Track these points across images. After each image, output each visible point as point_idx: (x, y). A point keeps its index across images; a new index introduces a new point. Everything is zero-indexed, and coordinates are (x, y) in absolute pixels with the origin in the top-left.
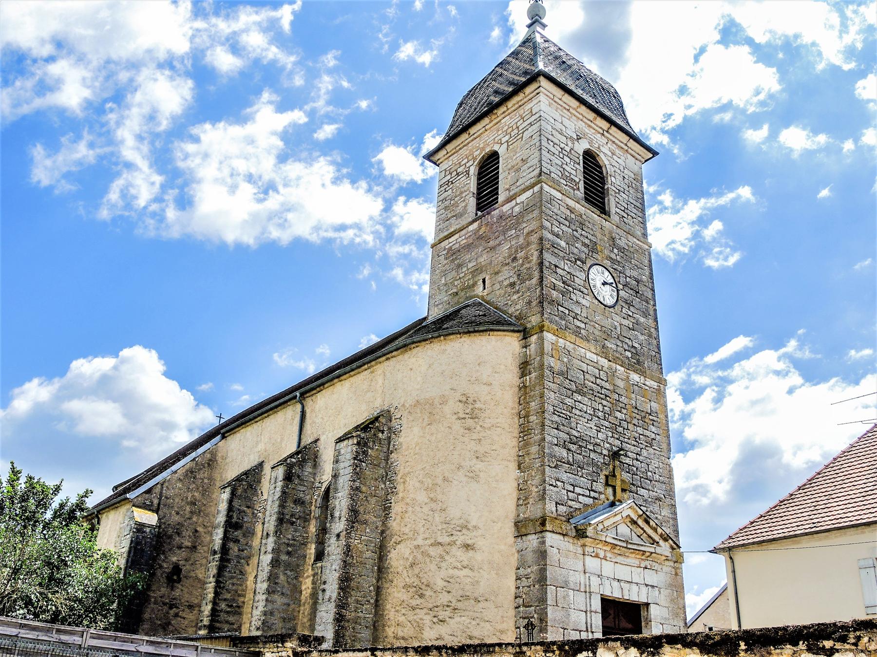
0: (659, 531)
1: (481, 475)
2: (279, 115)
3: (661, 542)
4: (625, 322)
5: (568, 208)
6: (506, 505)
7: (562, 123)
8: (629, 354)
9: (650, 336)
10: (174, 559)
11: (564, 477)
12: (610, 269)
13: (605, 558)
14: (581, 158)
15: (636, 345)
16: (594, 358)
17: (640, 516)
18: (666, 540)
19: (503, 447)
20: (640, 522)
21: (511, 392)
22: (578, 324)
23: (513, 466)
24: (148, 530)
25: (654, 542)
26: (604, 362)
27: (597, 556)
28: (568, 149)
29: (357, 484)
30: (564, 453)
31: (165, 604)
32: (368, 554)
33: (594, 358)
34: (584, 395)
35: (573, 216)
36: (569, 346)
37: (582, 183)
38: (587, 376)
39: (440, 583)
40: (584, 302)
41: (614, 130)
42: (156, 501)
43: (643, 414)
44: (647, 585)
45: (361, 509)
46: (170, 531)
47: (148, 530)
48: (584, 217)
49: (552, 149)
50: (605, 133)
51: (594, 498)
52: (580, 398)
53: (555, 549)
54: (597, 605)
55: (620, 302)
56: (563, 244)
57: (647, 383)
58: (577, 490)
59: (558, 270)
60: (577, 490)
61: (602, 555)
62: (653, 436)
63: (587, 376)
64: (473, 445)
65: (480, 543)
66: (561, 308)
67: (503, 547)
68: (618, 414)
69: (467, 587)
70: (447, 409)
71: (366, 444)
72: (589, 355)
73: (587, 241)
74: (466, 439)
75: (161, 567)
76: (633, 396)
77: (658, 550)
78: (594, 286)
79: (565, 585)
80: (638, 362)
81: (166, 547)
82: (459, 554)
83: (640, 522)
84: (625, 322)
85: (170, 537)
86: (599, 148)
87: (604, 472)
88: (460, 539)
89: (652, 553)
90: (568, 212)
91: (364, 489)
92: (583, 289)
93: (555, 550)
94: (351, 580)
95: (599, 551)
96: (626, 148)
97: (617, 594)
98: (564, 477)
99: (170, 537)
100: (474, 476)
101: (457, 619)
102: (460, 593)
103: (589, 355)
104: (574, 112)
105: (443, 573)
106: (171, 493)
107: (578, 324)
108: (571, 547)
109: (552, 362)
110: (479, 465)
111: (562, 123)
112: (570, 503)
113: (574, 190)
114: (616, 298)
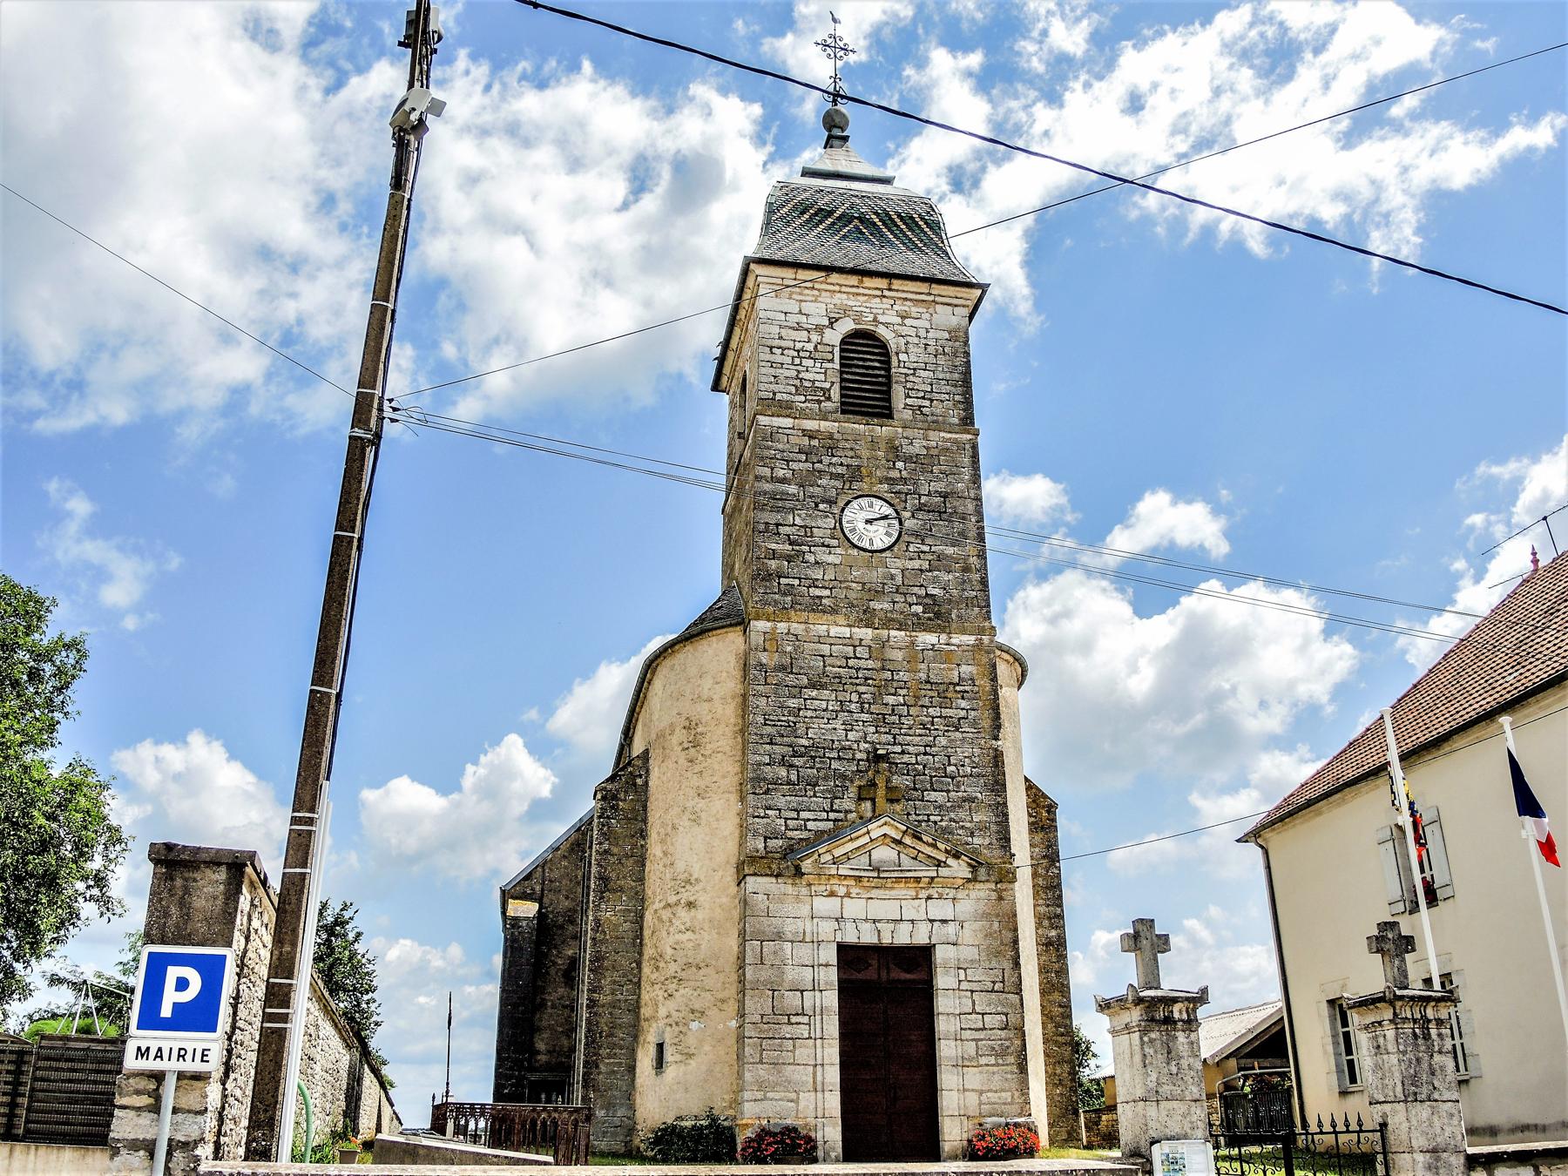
0: (942, 846)
1: (703, 815)
2: (1143, 54)
3: (950, 861)
4: (916, 564)
5: (805, 432)
6: (728, 850)
7: (800, 312)
8: (919, 609)
9: (966, 569)
10: (570, 952)
11: (781, 802)
12: (888, 496)
13: (848, 895)
14: (837, 350)
15: (935, 591)
16: (846, 632)
17: (904, 833)
18: (957, 856)
19: (724, 777)
20: (908, 840)
21: (733, 705)
22: (818, 592)
23: (734, 798)
24: (524, 923)
25: (939, 864)
26: (866, 634)
27: (832, 894)
28: (810, 347)
29: (606, 846)
30: (783, 772)
31: (565, 1007)
32: (627, 926)
33: (846, 632)
34: (823, 687)
35: (815, 442)
36: (798, 628)
37: (837, 387)
38: (829, 661)
39: (670, 951)
40: (831, 559)
41: (896, 284)
42: (538, 888)
43: (942, 687)
44: (932, 921)
45: (613, 875)
46: (561, 919)
47: (524, 923)
48: (836, 436)
49: (779, 359)
50: (886, 293)
51: (835, 820)
52: (814, 693)
53: (761, 897)
54: (830, 954)
55: (905, 538)
56: (792, 489)
57: (953, 641)
58: (804, 815)
59: (781, 529)
60: (804, 815)
61: (842, 891)
62: (963, 713)
63: (829, 661)
64: (695, 781)
65: (703, 899)
66: (783, 581)
67: (724, 900)
68: (891, 700)
69: (690, 953)
70: (675, 740)
71: (615, 797)
72: (834, 631)
73: (840, 470)
74: (689, 774)
75: (555, 963)
76: (923, 666)
77: (943, 871)
78: (853, 530)
79: (779, 936)
80: (938, 615)
81: (558, 940)
82: (682, 913)
83: (908, 840)
84: (916, 564)
85: (562, 927)
86: (875, 320)
87: (857, 783)
88: (685, 896)
89: (932, 878)
90: (806, 441)
91: (615, 850)
92: (827, 541)
93: (761, 897)
94: (604, 959)
95: (835, 888)
96: (931, 298)
97: (868, 937)
98: (781, 802)
99: (562, 927)
100: (696, 821)
101: (682, 991)
102: (685, 960)
103: (834, 631)
104: (824, 286)
105: (671, 940)
106: (556, 874)
107: (818, 592)
108: (790, 889)
109: (764, 658)
110: (702, 804)
111: (800, 312)
112: (790, 834)
113: (819, 402)
114: (896, 535)
